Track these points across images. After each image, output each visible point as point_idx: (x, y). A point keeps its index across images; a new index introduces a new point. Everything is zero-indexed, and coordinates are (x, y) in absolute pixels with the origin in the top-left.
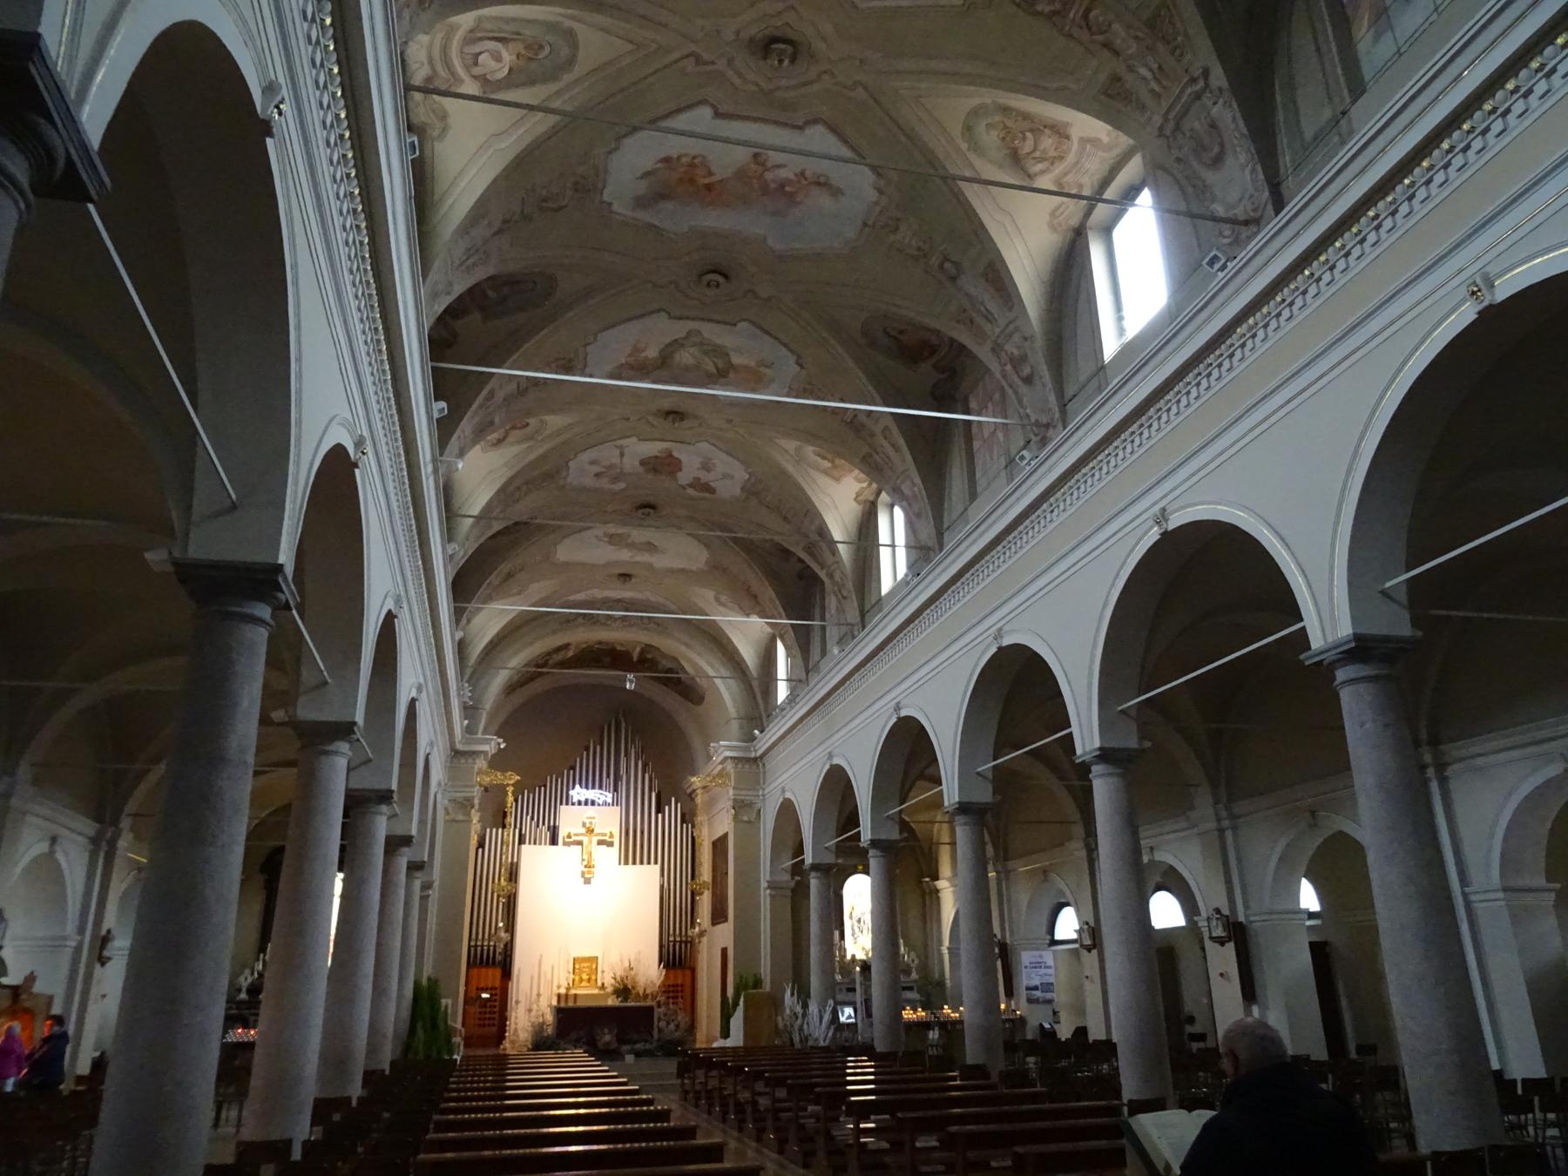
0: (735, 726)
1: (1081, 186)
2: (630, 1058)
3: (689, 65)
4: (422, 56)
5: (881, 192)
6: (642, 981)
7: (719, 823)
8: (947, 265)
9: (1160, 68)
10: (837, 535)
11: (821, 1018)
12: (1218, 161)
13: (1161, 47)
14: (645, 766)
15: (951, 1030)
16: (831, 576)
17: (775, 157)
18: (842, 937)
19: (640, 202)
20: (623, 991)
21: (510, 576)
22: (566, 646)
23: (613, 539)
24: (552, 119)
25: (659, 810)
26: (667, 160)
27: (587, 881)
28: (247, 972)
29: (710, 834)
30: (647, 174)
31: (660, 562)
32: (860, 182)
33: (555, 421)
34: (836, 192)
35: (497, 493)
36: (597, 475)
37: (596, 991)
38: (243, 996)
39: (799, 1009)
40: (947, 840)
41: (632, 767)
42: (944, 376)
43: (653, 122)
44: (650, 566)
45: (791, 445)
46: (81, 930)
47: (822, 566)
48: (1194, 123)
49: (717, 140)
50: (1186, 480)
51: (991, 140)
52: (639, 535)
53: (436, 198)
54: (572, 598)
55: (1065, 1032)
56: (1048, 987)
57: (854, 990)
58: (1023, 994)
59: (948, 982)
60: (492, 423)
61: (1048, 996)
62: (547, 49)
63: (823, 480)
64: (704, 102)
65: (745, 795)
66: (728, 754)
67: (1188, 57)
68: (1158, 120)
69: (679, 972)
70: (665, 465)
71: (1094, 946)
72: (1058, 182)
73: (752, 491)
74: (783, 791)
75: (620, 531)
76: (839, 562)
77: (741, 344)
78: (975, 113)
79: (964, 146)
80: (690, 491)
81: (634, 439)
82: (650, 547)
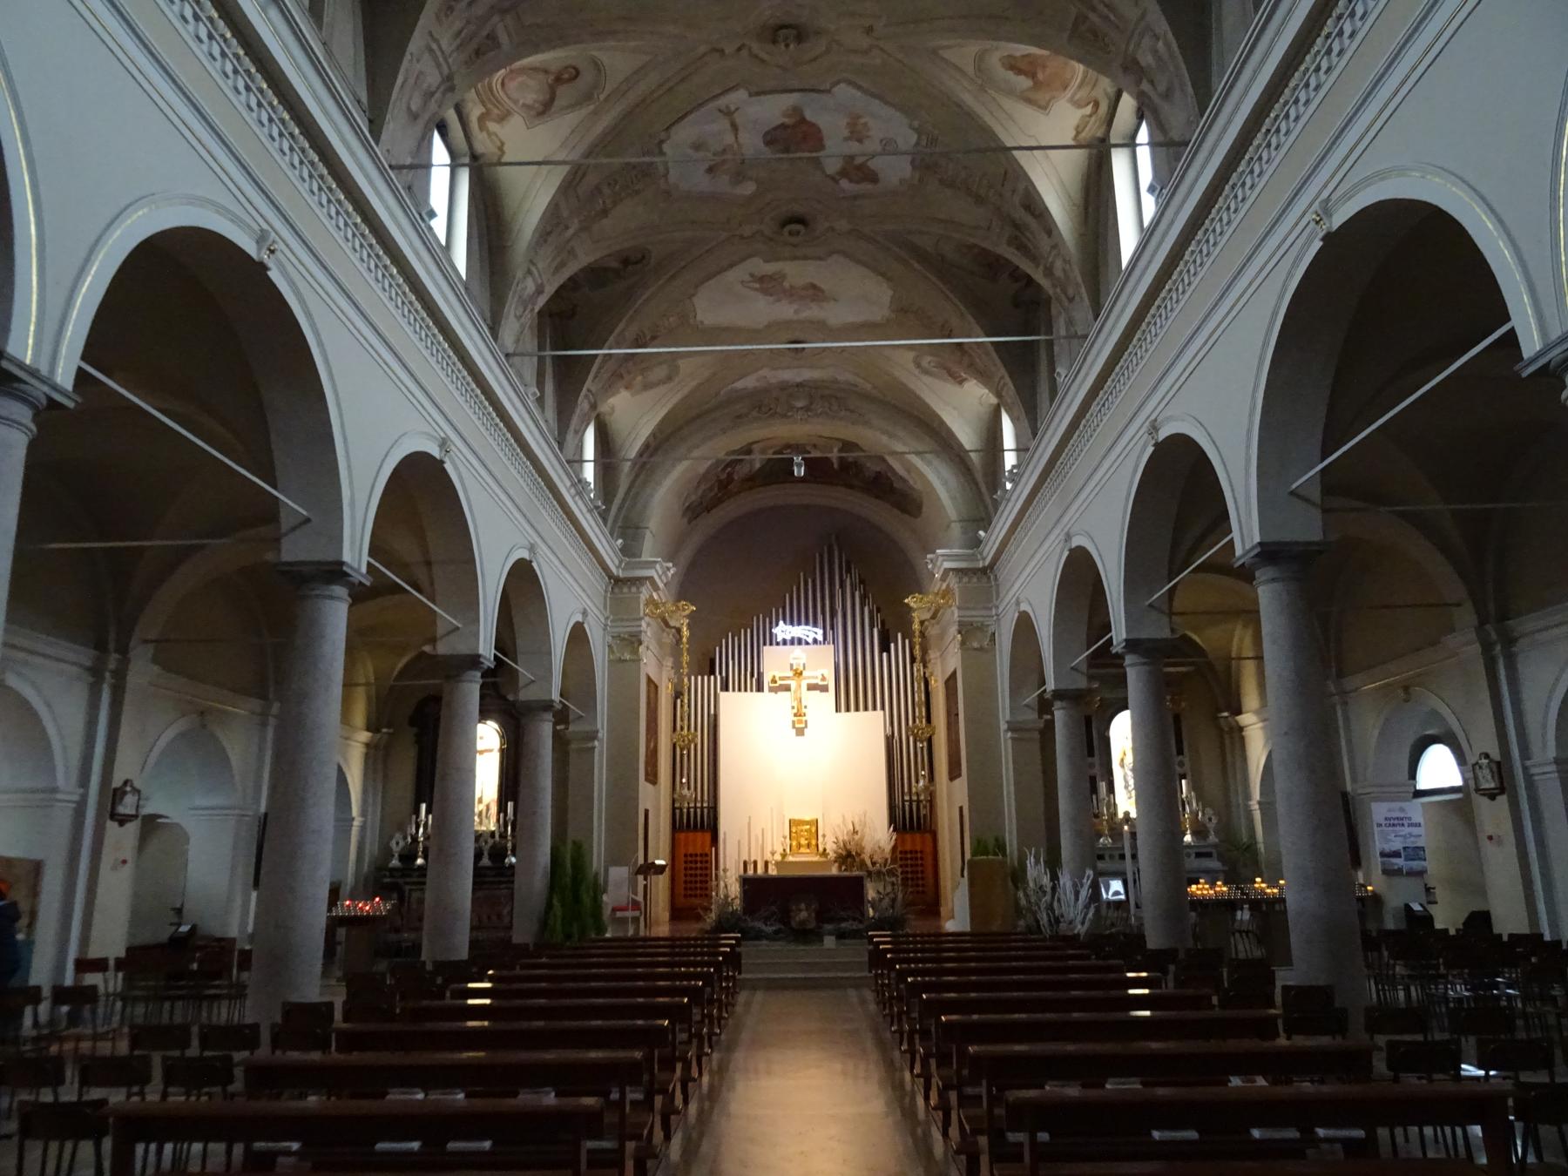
0: (956, 530)
2: (829, 942)
6: (868, 847)
7: (948, 660)
11: (1077, 894)
14: (863, 598)
15: (1270, 912)
16: (1049, 272)
18: (1111, 789)
20: (848, 856)
23: (768, 285)
25: (885, 648)
27: (800, 732)
28: (398, 836)
29: (943, 671)
37: (816, 859)
38: (395, 862)
39: (1046, 881)
40: (1248, 652)
41: (849, 599)
45: (964, 53)
46: (84, 781)
47: (1035, 259)
52: (796, 272)
55: (1447, 917)
56: (1416, 853)
57: (1122, 857)
58: (1377, 863)
59: (1261, 847)
61: (1416, 865)
65: (976, 615)
66: (947, 565)
69: (918, 836)
70: (795, 136)
71: (1501, 790)
74: (1018, 603)
75: (770, 268)
80: (844, 183)
81: (741, 95)
82: (815, 293)
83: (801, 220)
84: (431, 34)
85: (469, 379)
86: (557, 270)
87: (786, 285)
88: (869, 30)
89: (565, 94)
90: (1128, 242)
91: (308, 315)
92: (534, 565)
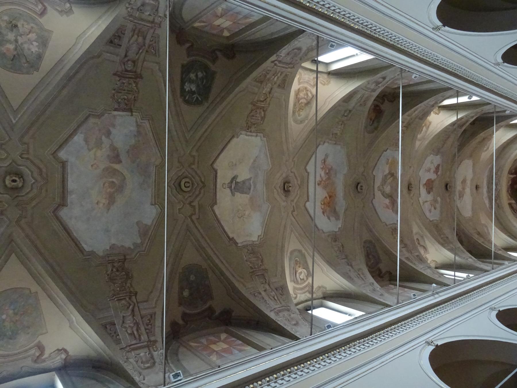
1: (314, 78)
3: (295, 213)
4: (303, 295)
5: (324, 142)
8: (346, 114)
9: (274, 75)
10: (454, 119)
12: (299, 49)
13: (268, 76)
17: (318, 179)
19: (337, 218)
21: (479, 234)
22: (510, 204)
23: (461, 196)
24: (316, 254)
26: (323, 213)
30: (329, 218)
31: (470, 175)
32: (323, 150)
33: (415, 229)
34: (327, 156)
35: (444, 247)
36: (435, 209)
42: (386, 99)
43: (312, 220)
44: (472, 180)
45: (418, 143)
48: (288, 59)
49: (317, 194)
50: (419, 25)
51: (303, 114)
53: (342, 289)
54: (488, 205)
60: (417, 256)
62: (297, 258)
63: (431, 128)
64: (305, 206)
67: (269, 68)
68: (289, 70)
70: (429, 186)
72: (313, 86)
73: (437, 151)
75: (458, 195)
76: (466, 116)
77: (381, 171)
78: (296, 121)
79: (306, 121)
80: (439, 173)
81: (420, 199)
82: (464, 182)
83: (446, 186)
84: (122, 349)
85: (424, 313)
86: (464, 252)
87: (461, 190)
88: (410, 167)
89: (422, 243)
90: (365, 57)
91: (507, 306)
92: (501, 309)
